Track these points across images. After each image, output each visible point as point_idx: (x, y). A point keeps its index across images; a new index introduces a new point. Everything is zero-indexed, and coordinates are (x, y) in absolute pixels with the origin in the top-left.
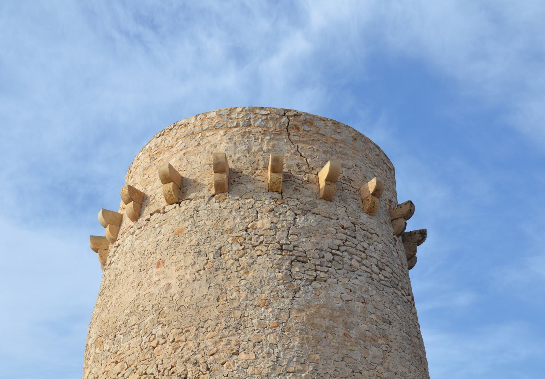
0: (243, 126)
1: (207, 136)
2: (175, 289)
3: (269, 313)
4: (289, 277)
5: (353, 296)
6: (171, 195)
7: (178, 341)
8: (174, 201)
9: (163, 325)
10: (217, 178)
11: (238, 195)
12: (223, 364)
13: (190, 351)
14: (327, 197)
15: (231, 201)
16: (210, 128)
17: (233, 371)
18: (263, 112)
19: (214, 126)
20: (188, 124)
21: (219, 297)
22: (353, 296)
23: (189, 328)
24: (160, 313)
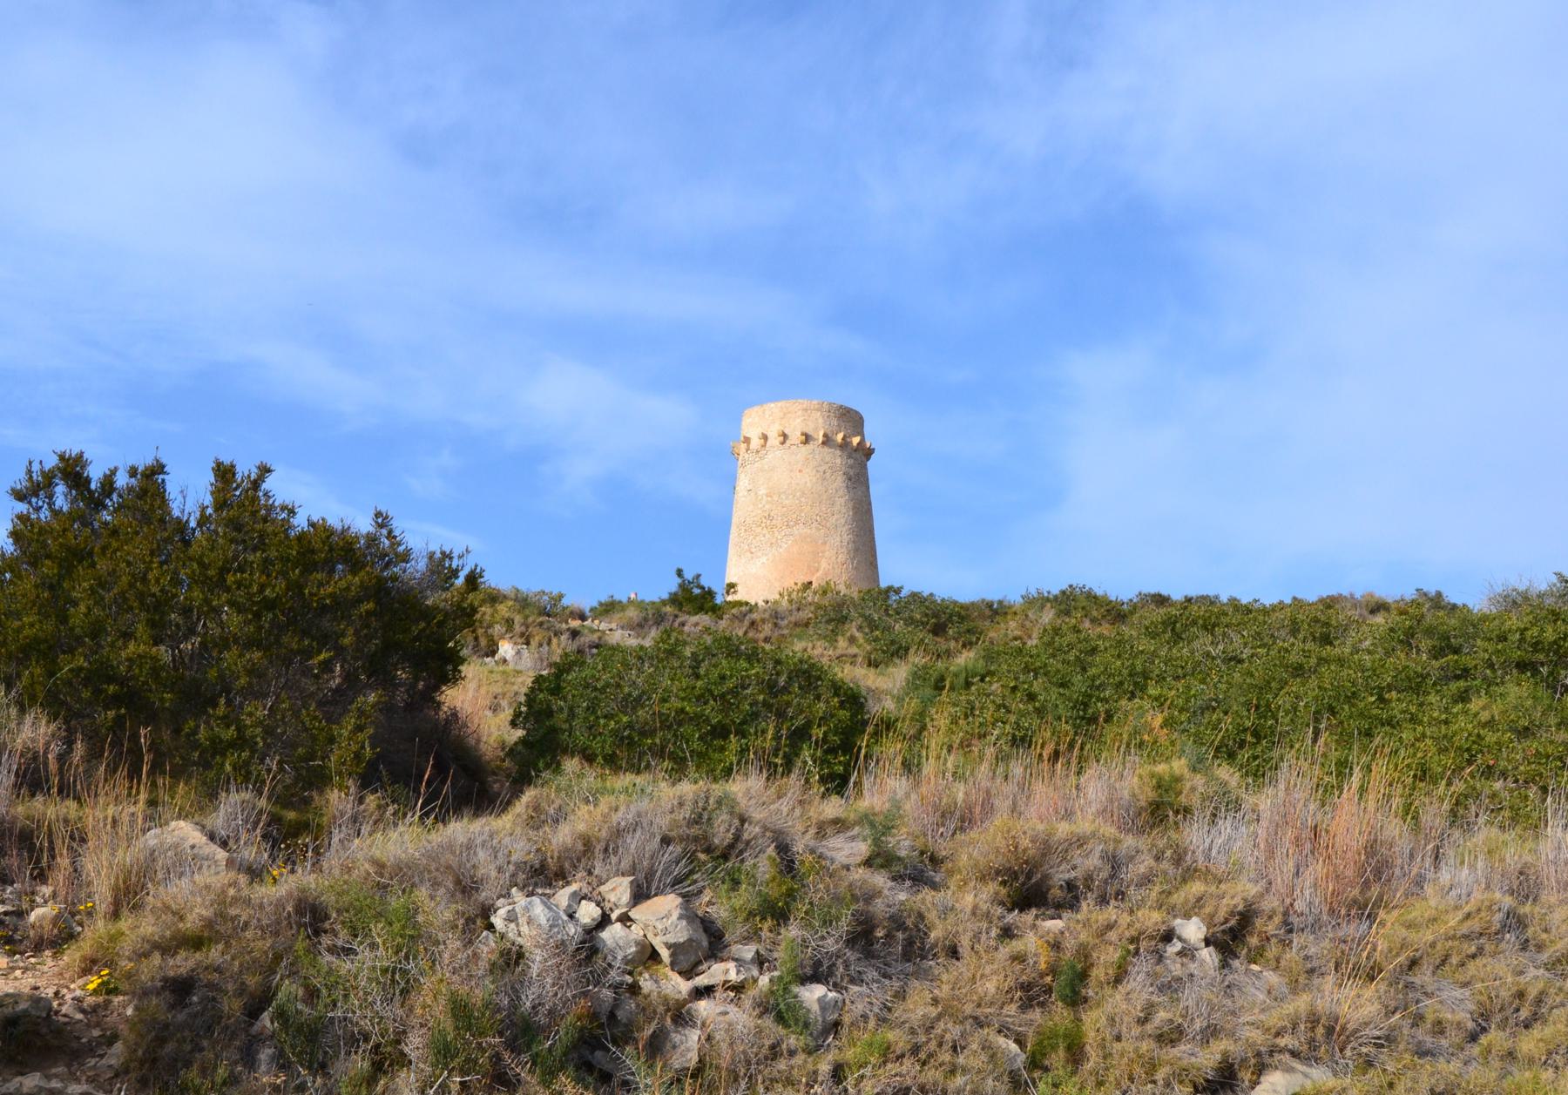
2: (809, 485)
3: (843, 500)
4: (847, 487)
14: (855, 451)
15: (826, 449)
24: (803, 493)
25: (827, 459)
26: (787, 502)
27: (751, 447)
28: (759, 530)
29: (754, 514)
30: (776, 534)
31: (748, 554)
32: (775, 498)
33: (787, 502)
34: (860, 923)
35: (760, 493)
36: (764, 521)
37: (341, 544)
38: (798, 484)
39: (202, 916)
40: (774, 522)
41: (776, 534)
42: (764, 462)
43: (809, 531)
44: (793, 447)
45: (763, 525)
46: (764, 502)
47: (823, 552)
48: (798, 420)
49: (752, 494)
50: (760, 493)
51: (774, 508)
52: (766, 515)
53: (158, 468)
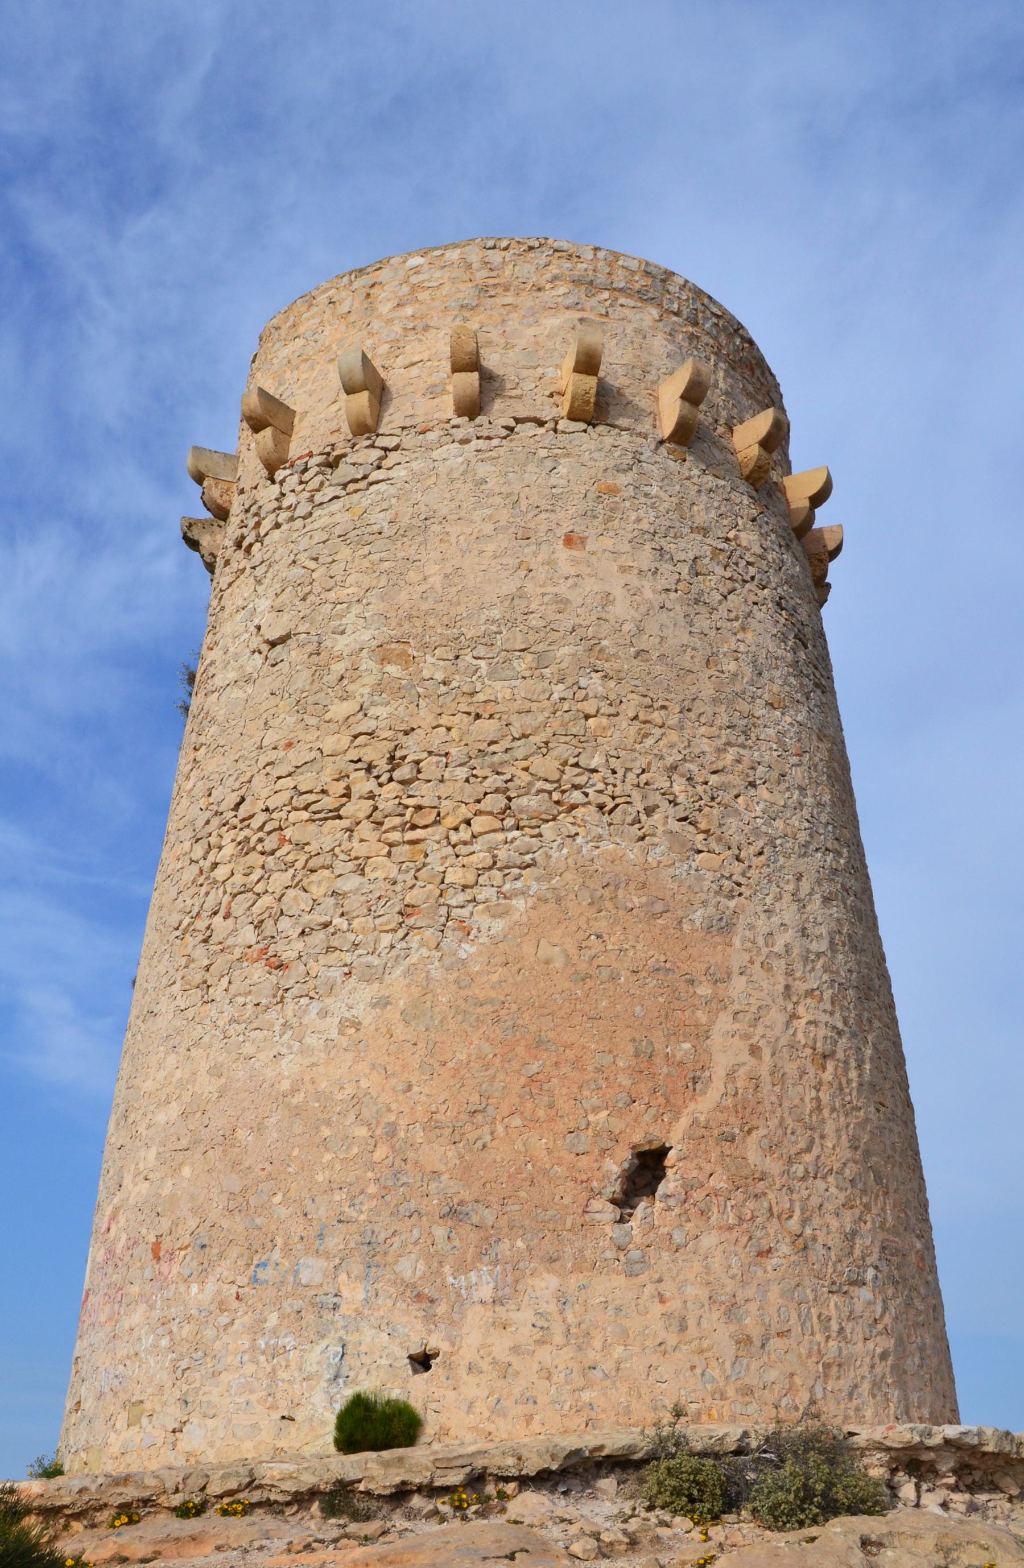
0: (686, 320)
1: (622, 306)
5: (114, 1217)
6: (588, 402)
7: (645, 722)
8: (582, 417)
9: (605, 677)
10: (685, 412)
11: (706, 463)
12: (737, 796)
13: (675, 751)
15: (692, 468)
16: (629, 291)
17: (755, 818)
18: (715, 310)
19: (639, 292)
20: (578, 257)
21: (708, 660)
22: (114, 1217)
23: (666, 703)
24: (594, 647)
25: (702, 516)
26: (500, 689)
27: (295, 449)
28: (329, 835)
29: (295, 757)
30: (437, 855)
31: (258, 972)
32: (433, 667)
33: (500, 689)
34: (618, 392)
35: (342, 644)
36: (363, 784)
37: (841, 1459)
38: (562, 603)
39: (876, 1414)
40: (424, 793)
41: (437, 855)
42: (362, 500)
43: (634, 854)
44: (527, 430)
45: (357, 808)
46: (361, 689)
47: (720, 978)
48: (552, 322)
49: (292, 654)
50: (342, 644)
51: (425, 716)
52: (376, 753)
53: (410, 1357)
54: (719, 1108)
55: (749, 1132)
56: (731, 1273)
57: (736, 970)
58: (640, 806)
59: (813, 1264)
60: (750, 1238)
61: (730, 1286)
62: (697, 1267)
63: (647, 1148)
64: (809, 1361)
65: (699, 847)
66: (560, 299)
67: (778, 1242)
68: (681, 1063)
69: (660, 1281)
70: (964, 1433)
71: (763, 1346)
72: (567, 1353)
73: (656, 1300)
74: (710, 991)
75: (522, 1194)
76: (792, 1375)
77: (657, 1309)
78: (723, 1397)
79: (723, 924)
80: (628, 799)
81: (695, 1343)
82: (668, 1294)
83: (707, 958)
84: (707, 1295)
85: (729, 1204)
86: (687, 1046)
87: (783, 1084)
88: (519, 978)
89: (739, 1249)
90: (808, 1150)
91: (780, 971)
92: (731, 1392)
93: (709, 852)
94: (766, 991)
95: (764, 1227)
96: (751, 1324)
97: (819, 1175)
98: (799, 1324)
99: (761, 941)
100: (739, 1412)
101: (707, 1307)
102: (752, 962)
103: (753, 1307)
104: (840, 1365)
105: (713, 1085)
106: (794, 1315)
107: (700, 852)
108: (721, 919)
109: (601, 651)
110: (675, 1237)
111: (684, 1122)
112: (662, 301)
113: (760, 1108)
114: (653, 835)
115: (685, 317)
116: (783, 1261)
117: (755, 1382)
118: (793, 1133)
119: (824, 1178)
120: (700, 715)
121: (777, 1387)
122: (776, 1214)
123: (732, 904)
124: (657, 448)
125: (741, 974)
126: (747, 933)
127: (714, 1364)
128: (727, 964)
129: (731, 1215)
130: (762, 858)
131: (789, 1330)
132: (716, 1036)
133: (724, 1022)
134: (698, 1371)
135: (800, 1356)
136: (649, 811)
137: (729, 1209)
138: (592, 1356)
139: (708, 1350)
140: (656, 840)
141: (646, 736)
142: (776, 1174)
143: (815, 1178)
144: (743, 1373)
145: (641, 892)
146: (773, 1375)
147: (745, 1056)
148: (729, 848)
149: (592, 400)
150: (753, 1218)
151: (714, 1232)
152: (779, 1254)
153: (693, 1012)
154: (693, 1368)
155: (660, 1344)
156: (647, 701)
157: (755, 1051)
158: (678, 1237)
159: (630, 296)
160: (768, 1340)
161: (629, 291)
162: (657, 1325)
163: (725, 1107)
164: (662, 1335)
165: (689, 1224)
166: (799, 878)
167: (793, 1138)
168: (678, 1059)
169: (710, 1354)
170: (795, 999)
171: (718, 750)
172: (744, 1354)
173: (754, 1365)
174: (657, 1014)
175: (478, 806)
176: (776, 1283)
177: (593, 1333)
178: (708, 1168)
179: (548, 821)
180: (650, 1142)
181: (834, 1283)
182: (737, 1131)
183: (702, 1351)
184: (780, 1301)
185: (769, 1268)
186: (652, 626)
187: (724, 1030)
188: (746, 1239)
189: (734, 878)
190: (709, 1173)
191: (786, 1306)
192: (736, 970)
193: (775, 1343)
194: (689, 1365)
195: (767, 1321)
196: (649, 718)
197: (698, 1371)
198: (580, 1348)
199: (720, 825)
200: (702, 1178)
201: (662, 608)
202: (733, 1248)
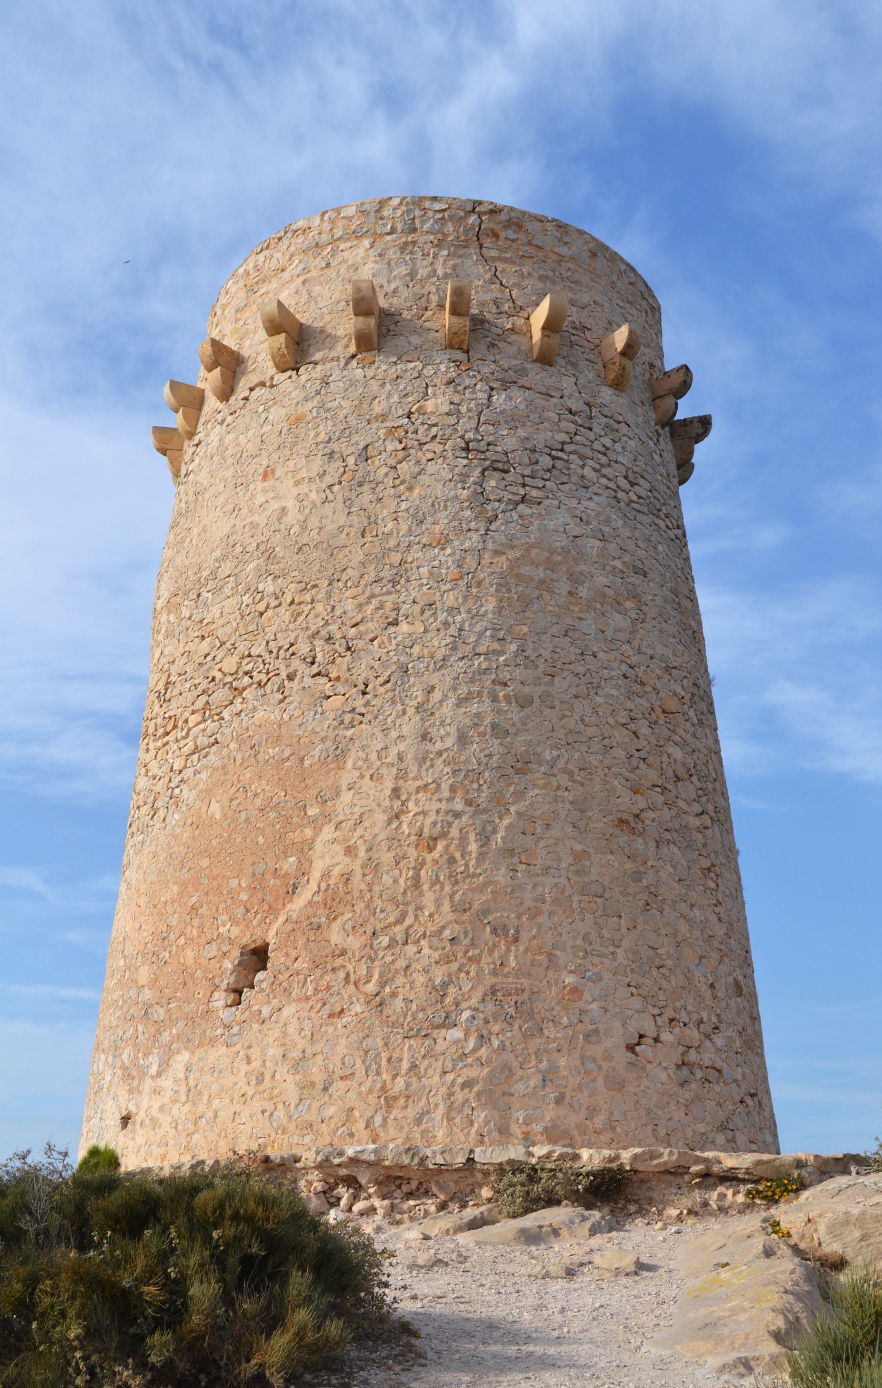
0: (402, 232)
6: (283, 355)
7: (300, 603)
10: (359, 325)
12: (372, 640)
20: (309, 228)
21: (364, 530)
54: (310, 903)
55: (335, 919)
56: (303, 1034)
57: (344, 787)
58: (284, 675)
59: (388, 1017)
60: (324, 1004)
61: (301, 1043)
62: (276, 1033)
63: (253, 946)
64: (371, 1096)
65: (328, 693)
66: (293, 272)
67: (352, 1003)
68: (286, 875)
69: (250, 1047)
70: (360, 1152)
71: (326, 1089)
72: (186, 1108)
73: (245, 1062)
74: (318, 811)
75: (179, 994)
76: (351, 1109)
77: (244, 1068)
78: (284, 1132)
79: (339, 751)
80: (277, 672)
81: (268, 1092)
82: (253, 1057)
83: (320, 784)
84: (281, 1053)
85: (309, 979)
86: (292, 859)
87: (376, 872)
88: (197, 832)
89: (312, 1014)
90: (400, 921)
91: (390, 777)
92: (292, 1127)
93: (335, 695)
94: (372, 798)
95: (338, 994)
96: (317, 1074)
97: (409, 941)
98: (363, 1068)
99: (373, 756)
100: (295, 1142)
101: (280, 1063)
102: (362, 777)
103: (319, 1059)
104: (408, 1097)
105: (309, 886)
106: (359, 1062)
107: (329, 697)
108: (338, 748)
109: (275, 556)
110: (263, 1012)
111: (281, 919)
112: (375, 230)
113: (349, 897)
114: (290, 696)
115: (400, 231)
116: (354, 1018)
117: (314, 1118)
118: (382, 911)
119: (418, 941)
120: (347, 581)
121: (333, 1121)
122: (352, 980)
123: (349, 733)
124: (347, 364)
125: (349, 789)
126: (360, 754)
127: (280, 1106)
128: (336, 785)
129: (310, 988)
130: (389, 686)
131: (354, 1073)
132: (318, 846)
133: (328, 832)
134: (267, 1114)
135: (360, 1094)
136: (291, 678)
137: (309, 983)
138: (202, 1108)
139: (277, 1096)
140: (291, 699)
141: (299, 614)
142: (356, 948)
143: (406, 943)
144: (304, 1111)
145: (274, 745)
146: (332, 1110)
147: (341, 858)
148: (355, 686)
149: (286, 352)
150: (328, 988)
151: (294, 1004)
152: (352, 1013)
153: (302, 831)
154: (263, 1112)
155: (243, 1095)
156: (303, 584)
157: (350, 851)
158: (266, 1012)
159: (348, 239)
160: (331, 1084)
161: (346, 236)
162: (242, 1082)
163: (315, 902)
164: (245, 1088)
165: (275, 1001)
166: (431, 690)
167: (382, 916)
168: (284, 871)
169: (279, 1099)
170: (403, 798)
171: (360, 605)
172: (306, 1096)
173: (316, 1105)
174: (273, 839)
175: (192, 707)
176: (345, 1037)
177: (203, 1092)
178: (293, 953)
179: (226, 707)
180: (254, 941)
181: (411, 1029)
182: (323, 919)
183: (271, 1099)
184: (345, 1051)
185: (339, 1026)
186: (314, 522)
187: (326, 839)
188: (319, 1005)
189: (357, 711)
190: (294, 958)
191: (351, 1055)
192: (344, 787)
193: (339, 1087)
194: (260, 1109)
195: (331, 1067)
196: (301, 600)
197: (267, 1114)
198: (194, 1104)
199: (349, 670)
200: (289, 963)
201: (324, 502)
202: (306, 1014)
